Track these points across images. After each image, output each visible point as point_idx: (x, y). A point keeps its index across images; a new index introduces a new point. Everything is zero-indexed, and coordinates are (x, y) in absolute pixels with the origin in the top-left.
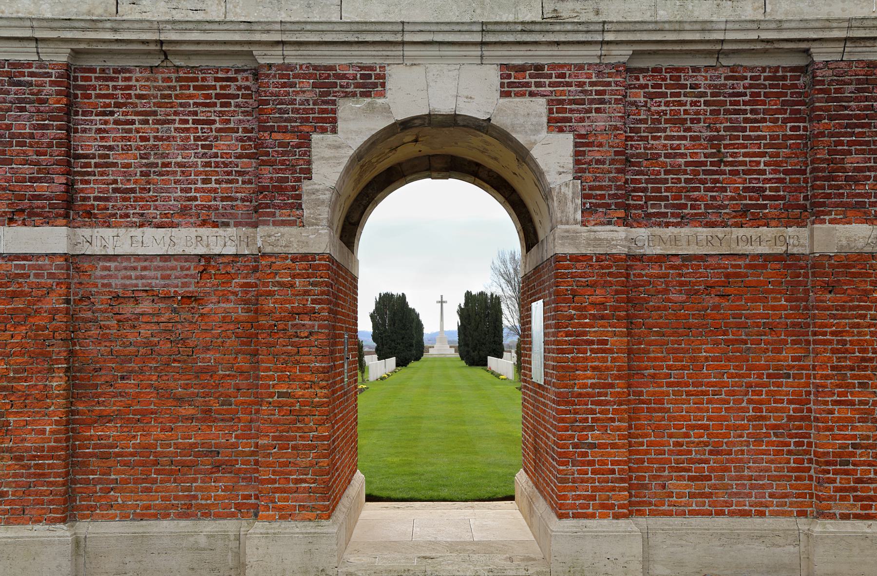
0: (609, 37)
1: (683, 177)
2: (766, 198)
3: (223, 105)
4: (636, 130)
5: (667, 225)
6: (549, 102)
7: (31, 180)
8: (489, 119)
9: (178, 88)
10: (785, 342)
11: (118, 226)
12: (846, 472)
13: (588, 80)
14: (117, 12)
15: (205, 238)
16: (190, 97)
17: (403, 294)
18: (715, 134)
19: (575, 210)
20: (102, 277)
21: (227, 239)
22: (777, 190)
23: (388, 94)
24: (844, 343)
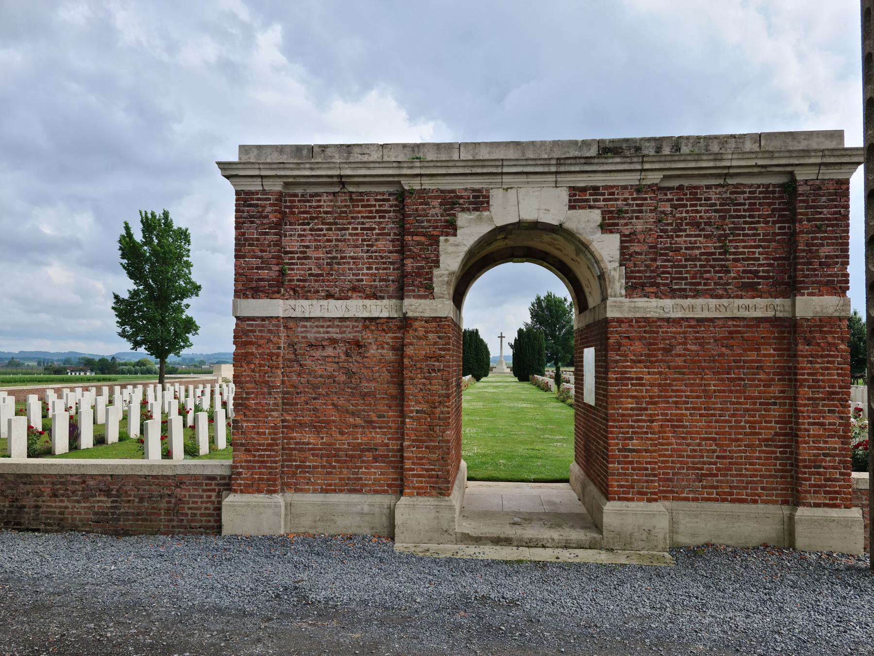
6: (603, 213)
12: (819, 474)
13: (630, 197)
15: (368, 306)
16: (359, 212)
23: (491, 208)
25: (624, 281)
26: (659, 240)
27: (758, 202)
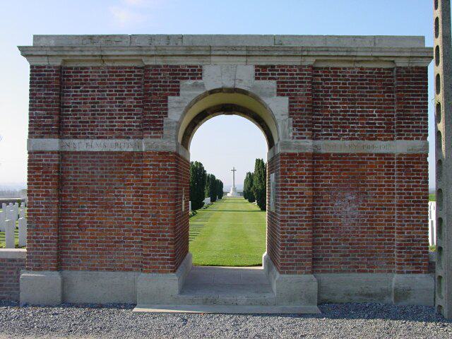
2: (376, 127)
6: (278, 82)
11: (81, 138)
16: (114, 80)
22: (381, 124)
23: (203, 78)
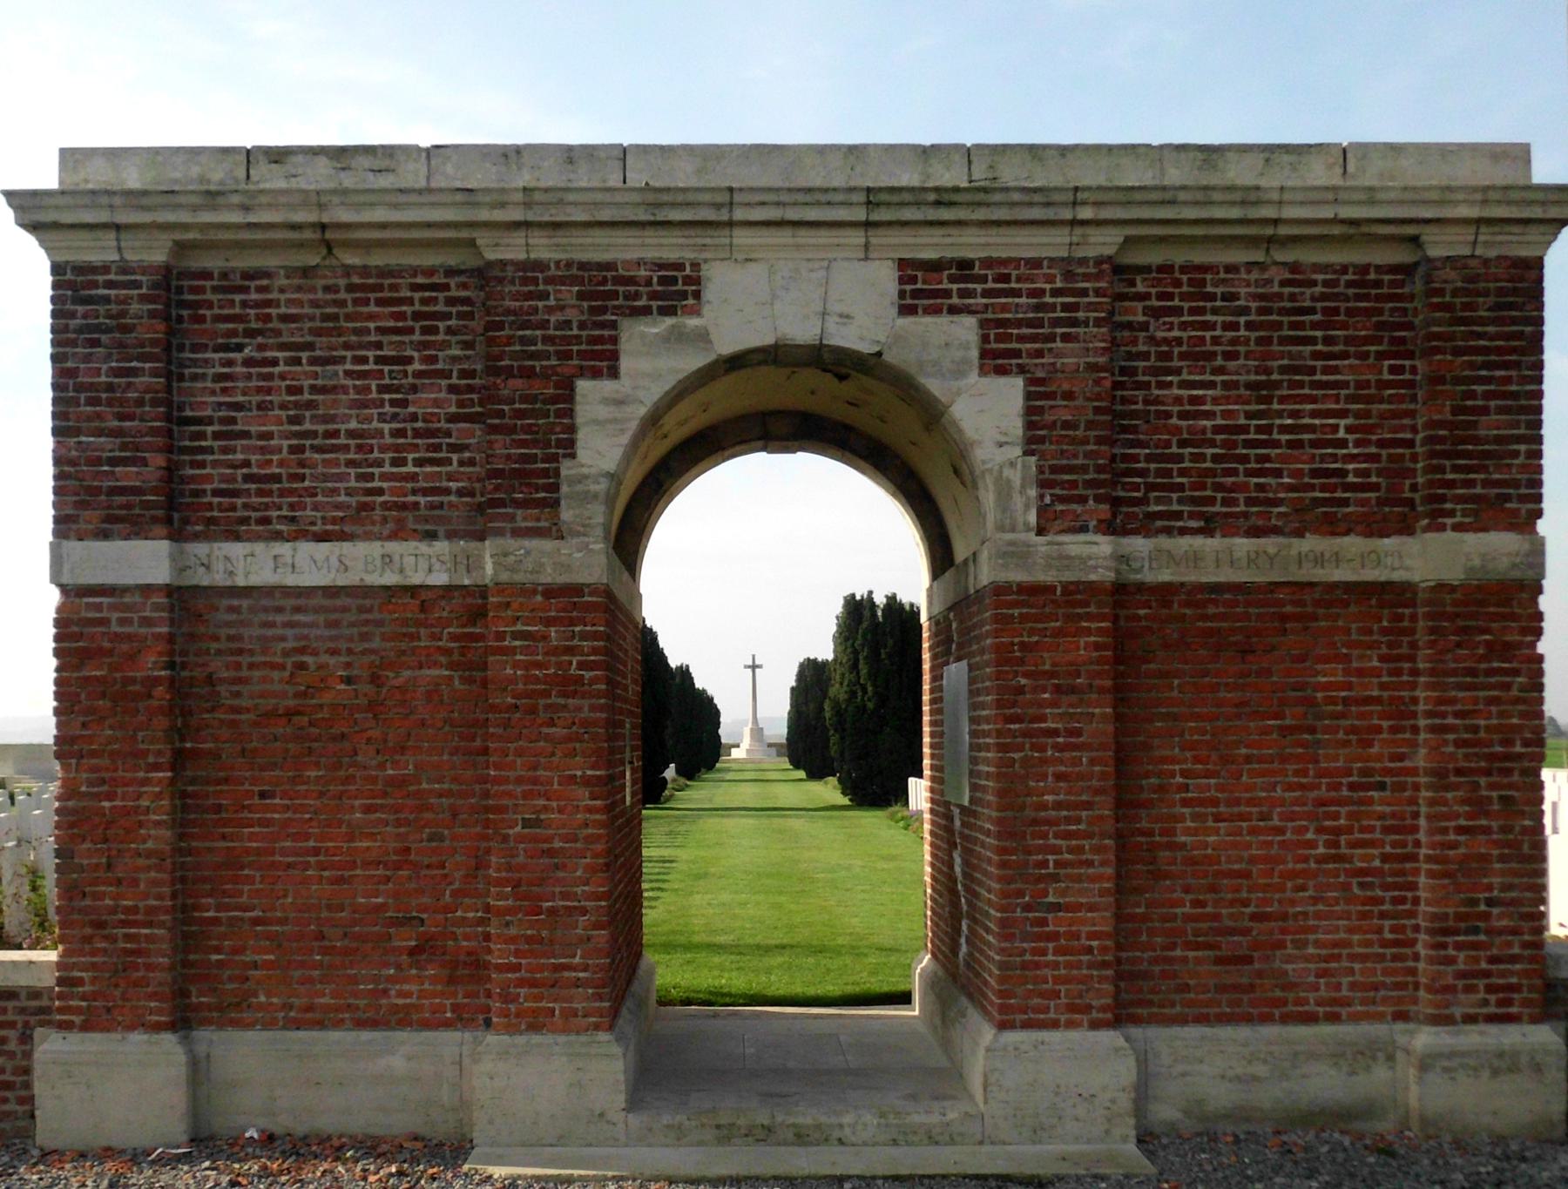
0: (1086, 213)
1: (1210, 451)
3: (426, 331)
4: (1132, 372)
5: (1183, 532)
6: (983, 324)
7: (113, 462)
8: (879, 354)
9: (350, 303)
10: (1379, 730)
12: (1475, 946)
13: (1048, 286)
14: (248, 177)
15: (396, 558)
16: (371, 317)
17: (870, 593)
18: (1263, 378)
19: (1027, 507)
20: (228, 624)
21: (434, 560)
23: (706, 310)
24: (1476, 729)
25: (1033, 492)
26: (1119, 393)
27: (1343, 305)
